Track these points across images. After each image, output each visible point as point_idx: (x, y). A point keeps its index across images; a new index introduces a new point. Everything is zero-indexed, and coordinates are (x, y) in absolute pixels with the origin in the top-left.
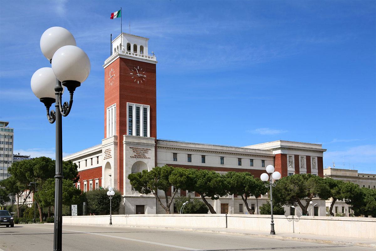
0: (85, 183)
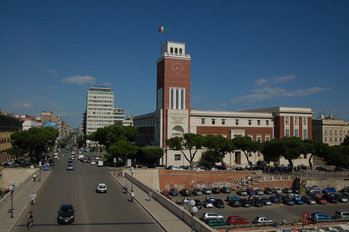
0: (147, 135)
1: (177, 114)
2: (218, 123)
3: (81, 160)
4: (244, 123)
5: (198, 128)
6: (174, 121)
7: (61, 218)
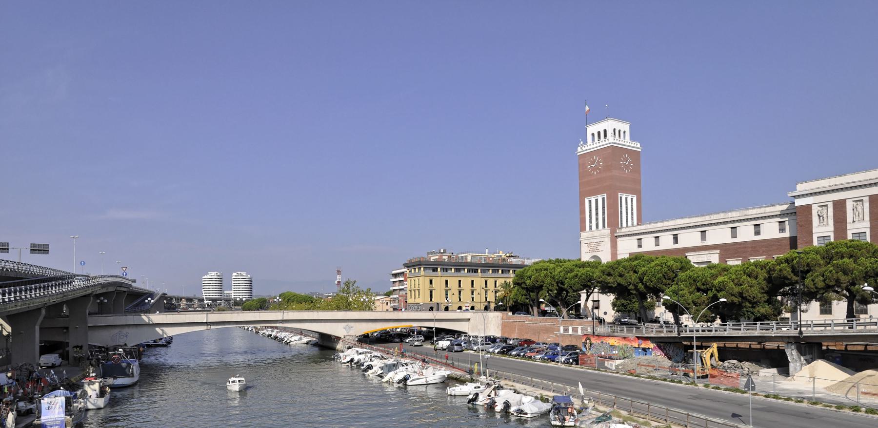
1: (592, 238)
2: (667, 243)
3: (243, 391)
4: (720, 236)
5: (630, 254)
7: (794, 287)
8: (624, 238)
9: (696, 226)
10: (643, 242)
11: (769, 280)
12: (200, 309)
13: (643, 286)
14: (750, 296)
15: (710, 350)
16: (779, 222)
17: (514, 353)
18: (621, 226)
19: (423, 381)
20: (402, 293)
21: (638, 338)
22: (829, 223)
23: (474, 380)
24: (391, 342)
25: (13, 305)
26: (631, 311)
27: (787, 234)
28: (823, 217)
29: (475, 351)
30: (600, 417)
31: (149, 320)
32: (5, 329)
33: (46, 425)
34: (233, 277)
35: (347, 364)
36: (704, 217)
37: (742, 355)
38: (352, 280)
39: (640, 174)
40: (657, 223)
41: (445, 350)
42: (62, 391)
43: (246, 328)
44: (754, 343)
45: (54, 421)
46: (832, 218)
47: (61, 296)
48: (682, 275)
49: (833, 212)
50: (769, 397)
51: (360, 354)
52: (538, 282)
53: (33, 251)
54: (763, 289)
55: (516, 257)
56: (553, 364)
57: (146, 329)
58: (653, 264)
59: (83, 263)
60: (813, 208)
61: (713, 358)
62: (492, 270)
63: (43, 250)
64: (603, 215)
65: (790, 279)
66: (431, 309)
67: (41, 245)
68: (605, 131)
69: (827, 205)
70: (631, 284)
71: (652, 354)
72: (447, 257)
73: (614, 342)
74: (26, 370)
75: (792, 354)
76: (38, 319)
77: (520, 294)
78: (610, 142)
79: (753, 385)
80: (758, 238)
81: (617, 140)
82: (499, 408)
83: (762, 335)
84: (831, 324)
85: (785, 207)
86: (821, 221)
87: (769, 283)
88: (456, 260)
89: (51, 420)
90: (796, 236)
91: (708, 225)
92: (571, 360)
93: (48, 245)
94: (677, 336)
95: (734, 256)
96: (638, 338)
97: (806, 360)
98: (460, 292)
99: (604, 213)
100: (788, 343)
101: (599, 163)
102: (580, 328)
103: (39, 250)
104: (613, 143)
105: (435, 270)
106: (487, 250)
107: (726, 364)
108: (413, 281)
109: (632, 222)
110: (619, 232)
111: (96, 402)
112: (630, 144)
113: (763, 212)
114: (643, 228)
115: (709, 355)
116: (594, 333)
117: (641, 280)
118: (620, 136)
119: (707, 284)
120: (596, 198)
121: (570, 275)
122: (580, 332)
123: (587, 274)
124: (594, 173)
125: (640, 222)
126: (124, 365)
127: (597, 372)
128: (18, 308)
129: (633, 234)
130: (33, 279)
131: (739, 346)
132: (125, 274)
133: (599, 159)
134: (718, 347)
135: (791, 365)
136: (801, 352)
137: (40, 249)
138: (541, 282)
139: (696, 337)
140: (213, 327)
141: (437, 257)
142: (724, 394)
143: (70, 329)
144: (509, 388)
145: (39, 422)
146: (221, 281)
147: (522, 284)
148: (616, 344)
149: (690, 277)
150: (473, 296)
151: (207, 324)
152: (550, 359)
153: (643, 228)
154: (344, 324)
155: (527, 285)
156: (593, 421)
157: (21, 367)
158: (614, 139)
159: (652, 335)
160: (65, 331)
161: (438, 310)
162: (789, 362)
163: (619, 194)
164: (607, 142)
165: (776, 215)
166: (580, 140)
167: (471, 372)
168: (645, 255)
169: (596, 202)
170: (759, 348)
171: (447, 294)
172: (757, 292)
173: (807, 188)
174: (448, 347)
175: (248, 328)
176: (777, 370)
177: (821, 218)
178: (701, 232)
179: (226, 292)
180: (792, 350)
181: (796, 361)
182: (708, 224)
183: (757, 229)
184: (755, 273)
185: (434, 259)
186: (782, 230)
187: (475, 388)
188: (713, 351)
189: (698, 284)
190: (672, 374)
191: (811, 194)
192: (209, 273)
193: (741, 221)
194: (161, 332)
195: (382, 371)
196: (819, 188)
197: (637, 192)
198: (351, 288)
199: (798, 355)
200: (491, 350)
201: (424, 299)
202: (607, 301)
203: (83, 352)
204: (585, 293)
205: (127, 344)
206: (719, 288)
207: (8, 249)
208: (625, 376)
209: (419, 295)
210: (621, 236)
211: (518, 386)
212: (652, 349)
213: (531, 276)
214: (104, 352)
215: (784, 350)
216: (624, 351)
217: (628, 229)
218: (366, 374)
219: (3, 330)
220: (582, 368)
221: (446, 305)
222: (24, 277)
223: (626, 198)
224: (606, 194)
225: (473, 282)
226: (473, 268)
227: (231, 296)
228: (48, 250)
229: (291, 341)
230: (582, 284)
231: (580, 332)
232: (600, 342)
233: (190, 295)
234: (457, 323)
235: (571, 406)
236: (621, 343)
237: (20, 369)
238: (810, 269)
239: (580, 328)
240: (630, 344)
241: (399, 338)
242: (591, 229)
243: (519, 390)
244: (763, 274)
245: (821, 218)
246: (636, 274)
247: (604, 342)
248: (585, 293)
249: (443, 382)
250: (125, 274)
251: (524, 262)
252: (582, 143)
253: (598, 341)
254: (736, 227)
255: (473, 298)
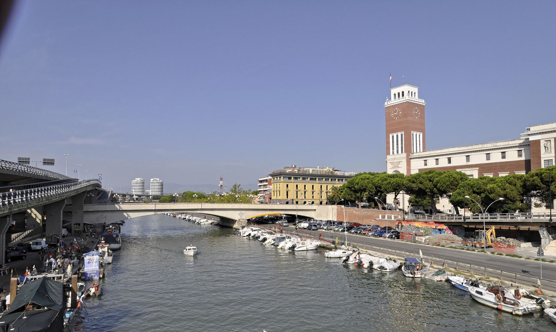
1: (394, 159)
2: (443, 163)
3: (196, 255)
4: (479, 159)
5: (420, 170)
6: (392, 166)
8: (414, 160)
9: (463, 153)
10: (428, 162)
11: (524, 186)
12: (132, 201)
13: (436, 190)
14: (512, 197)
15: (490, 231)
16: (518, 151)
17: (353, 231)
18: (413, 152)
19: (305, 248)
20: (267, 192)
21: (436, 222)
22: (552, 152)
23: (337, 248)
24: (267, 223)
25: (55, 197)
26: (421, 205)
27: (523, 158)
28: (548, 148)
29: (325, 229)
30: (437, 272)
31: (120, 208)
32: (33, 212)
33: (87, 273)
34: (151, 182)
35: (246, 237)
36: (468, 147)
37: (508, 234)
38: (238, 184)
39: (424, 119)
40: (437, 150)
41: (306, 229)
42: (95, 252)
43: (166, 214)
44: (512, 226)
45: (92, 271)
46: (554, 148)
47: (76, 192)
48: (461, 183)
49: (555, 145)
50: (538, 260)
51: (254, 231)
52: (363, 186)
53: (45, 163)
54: (520, 192)
55: (339, 171)
56: (382, 238)
57: (117, 213)
58: (443, 176)
59: (75, 171)
60: (541, 142)
61: (492, 235)
62: (325, 179)
63: (26, 162)
64: (401, 145)
65: (540, 186)
66: (287, 203)
67: (21, 158)
68: (403, 92)
69: (550, 140)
70: (427, 188)
71: (445, 233)
72: (297, 170)
73: (418, 225)
74: (55, 239)
75: (544, 233)
76: (63, 206)
77: (347, 194)
78: (406, 99)
79: (542, 252)
80: (504, 160)
81: (411, 98)
82: (366, 265)
83: (524, 221)
84: (544, 215)
85: (522, 141)
86: (546, 150)
87: (524, 188)
88: (303, 172)
89: (91, 270)
90: (530, 160)
91: (471, 152)
92: (394, 236)
93: (54, 160)
94: (463, 221)
95: (503, 170)
96: (436, 222)
97: (552, 237)
98: (305, 192)
99: (402, 143)
100: (541, 226)
101: (399, 112)
102: (393, 216)
103: (48, 163)
104: (408, 100)
105: (290, 178)
106: (318, 166)
107: (498, 239)
108: (275, 185)
109: (420, 150)
110: (412, 156)
111: (107, 259)
112: (419, 101)
113: (507, 144)
114: (427, 153)
115: (489, 233)
116: (404, 219)
117: (435, 186)
118: (412, 96)
119: (480, 189)
120: (397, 134)
121: (385, 182)
122: (393, 219)
123: (396, 182)
124: (395, 118)
125: (424, 150)
126: (114, 236)
127: (414, 244)
128: (57, 199)
129: (422, 157)
130: (55, 181)
131: (502, 228)
132: (100, 178)
133: (399, 110)
134: (495, 229)
135: (543, 240)
136: (550, 232)
137: (49, 162)
138: (365, 187)
139: (485, 222)
140: (158, 213)
141: (291, 170)
142: (507, 258)
143: (73, 213)
144: (365, 253)
145: (83, 271)
146: (143, 184)
147: (352, 187)
148: (420, 226)
149: (469, 184)
150: (313, 195)
151: (155, 210)
152: (379, 235)
153: (427, 153)
154: (239, 212)
155: (355, 189)
156: (433, 275)
157: (51, 237)
158: (409, 98)
159: (446, 221)
160: (69, 214)
161: (293, 203)
162: (541, 238)
163: (412, 132)
164: (404, 99)
165: (516, 146)
166: (387, 98)
167: (334, 243)
168: (435, 170)
169: (397, 137)
170: (515, 229)
171: (297, 194)
172: (516, 194)
173: (537, 130)
174: (308, 227)
175: (167, 214)
176: (532, 244)
177: (547, 148)
178: (466, 156)
179: (146, 191)
180: (544, 231)
181: (546, 238)
182: (471, 151)
183: (504, 155)
184: (514, 182)
185: (289, 172)
186: (520, 155)
187: (343, 253)
188: (492, 231)
189: (474, 189)
190: (464, 245)
191: (540, 133)
192: (136, 179)
193: (493, 149)
194: (126, 216)
195: (274, 242)
196: (545, 129)
197: (422, 130)
198: (237, 189)
199: (547, 234)
200: (336, 229)
201: (283, 196)
202: (404, 199)
203: (80, 227)
204: (394, 194)
205: (106, 223)
206: (491, 191)
207: (29, 162)
208: (434, 246)
209: (277, 194)
210: (413, 158)
211: (370, 252)
212: (445, 230)
213: (359, 183)
214: (93, 228)
215: (538, 231)
216: (426, 231)
217: (418, 154)
218: (263, 243)
219: (32, 213)
220: (403, 241)
221: (296, 200)
222: (50, 180)
223: (416, 134)
224: (403, 132)
225: (313, 186)
226: (313, 177)
227: (150, 193)
228: (54, 163)
229: (201, 223)
230: (394, 188)
231: (393, 219)
232: (408, 225)
233: (125, 193)
234: (308, 212)
235: (419, 265)
236: (424, 226)
237: (51, 237)
238: (554, 180)
239: (393, 216)
240: (430, 226)
241: (271, 221)
242: (393, 153)
243: (371, 254)
244: (519, 183)
245: (547, 148)
246: (431, 182)
247: (412, 225)
248: (394, 194)
249: (316, 249)
250: (100, 178)
251: (345, 174)
252: (388, 99)
253: (407, 224)
254: (489, 154)
255: (313, 197)
